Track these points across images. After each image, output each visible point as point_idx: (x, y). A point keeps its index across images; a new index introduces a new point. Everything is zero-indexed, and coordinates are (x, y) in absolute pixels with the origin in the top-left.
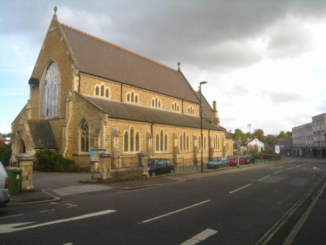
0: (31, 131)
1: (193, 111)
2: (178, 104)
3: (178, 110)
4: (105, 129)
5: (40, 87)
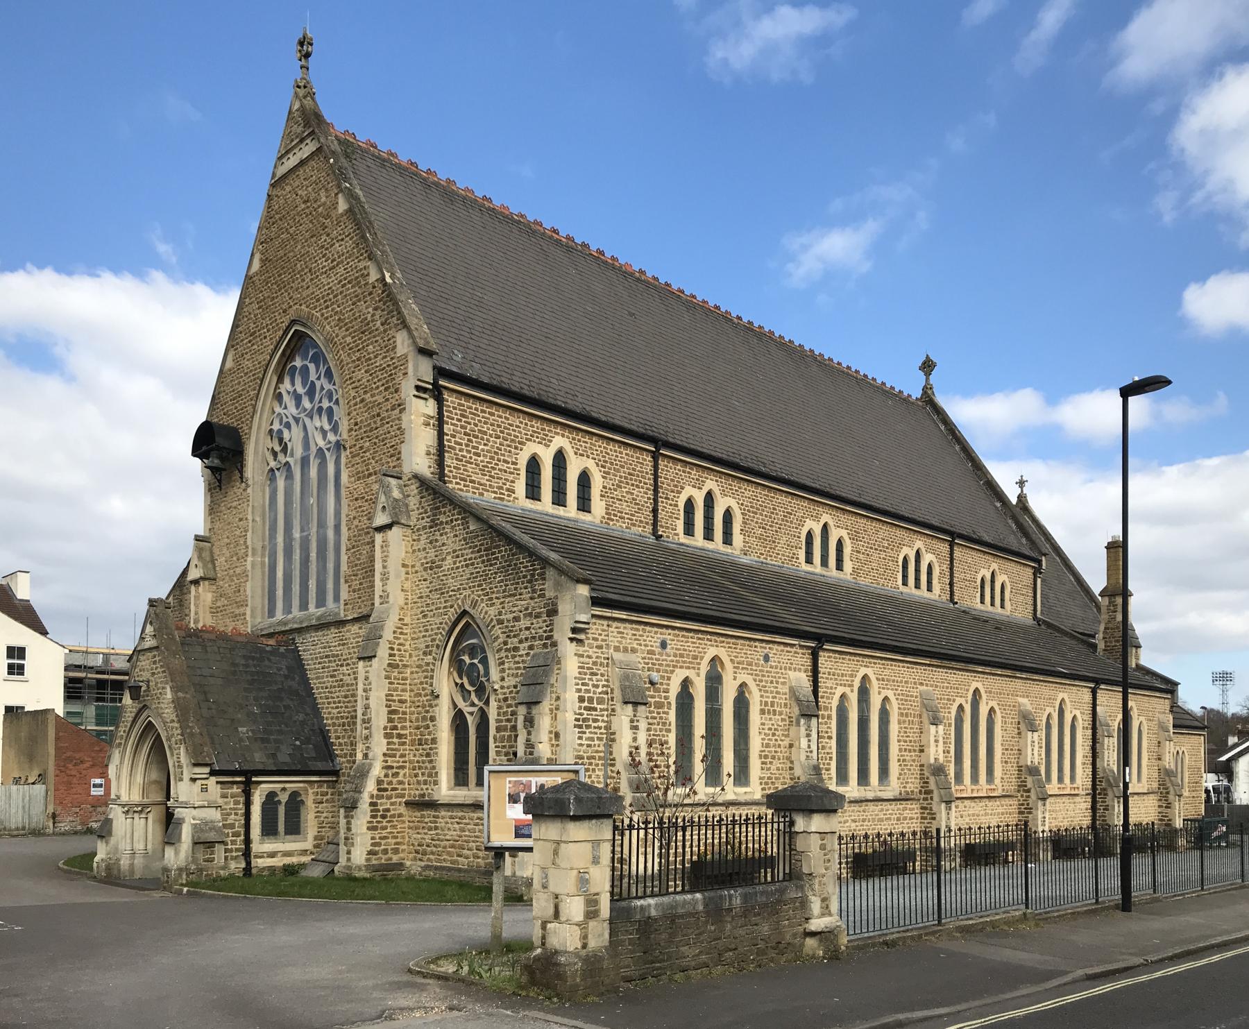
1: (1001, 591)
2: (927, 558)
3: (929, 589)
5: (249, 472)
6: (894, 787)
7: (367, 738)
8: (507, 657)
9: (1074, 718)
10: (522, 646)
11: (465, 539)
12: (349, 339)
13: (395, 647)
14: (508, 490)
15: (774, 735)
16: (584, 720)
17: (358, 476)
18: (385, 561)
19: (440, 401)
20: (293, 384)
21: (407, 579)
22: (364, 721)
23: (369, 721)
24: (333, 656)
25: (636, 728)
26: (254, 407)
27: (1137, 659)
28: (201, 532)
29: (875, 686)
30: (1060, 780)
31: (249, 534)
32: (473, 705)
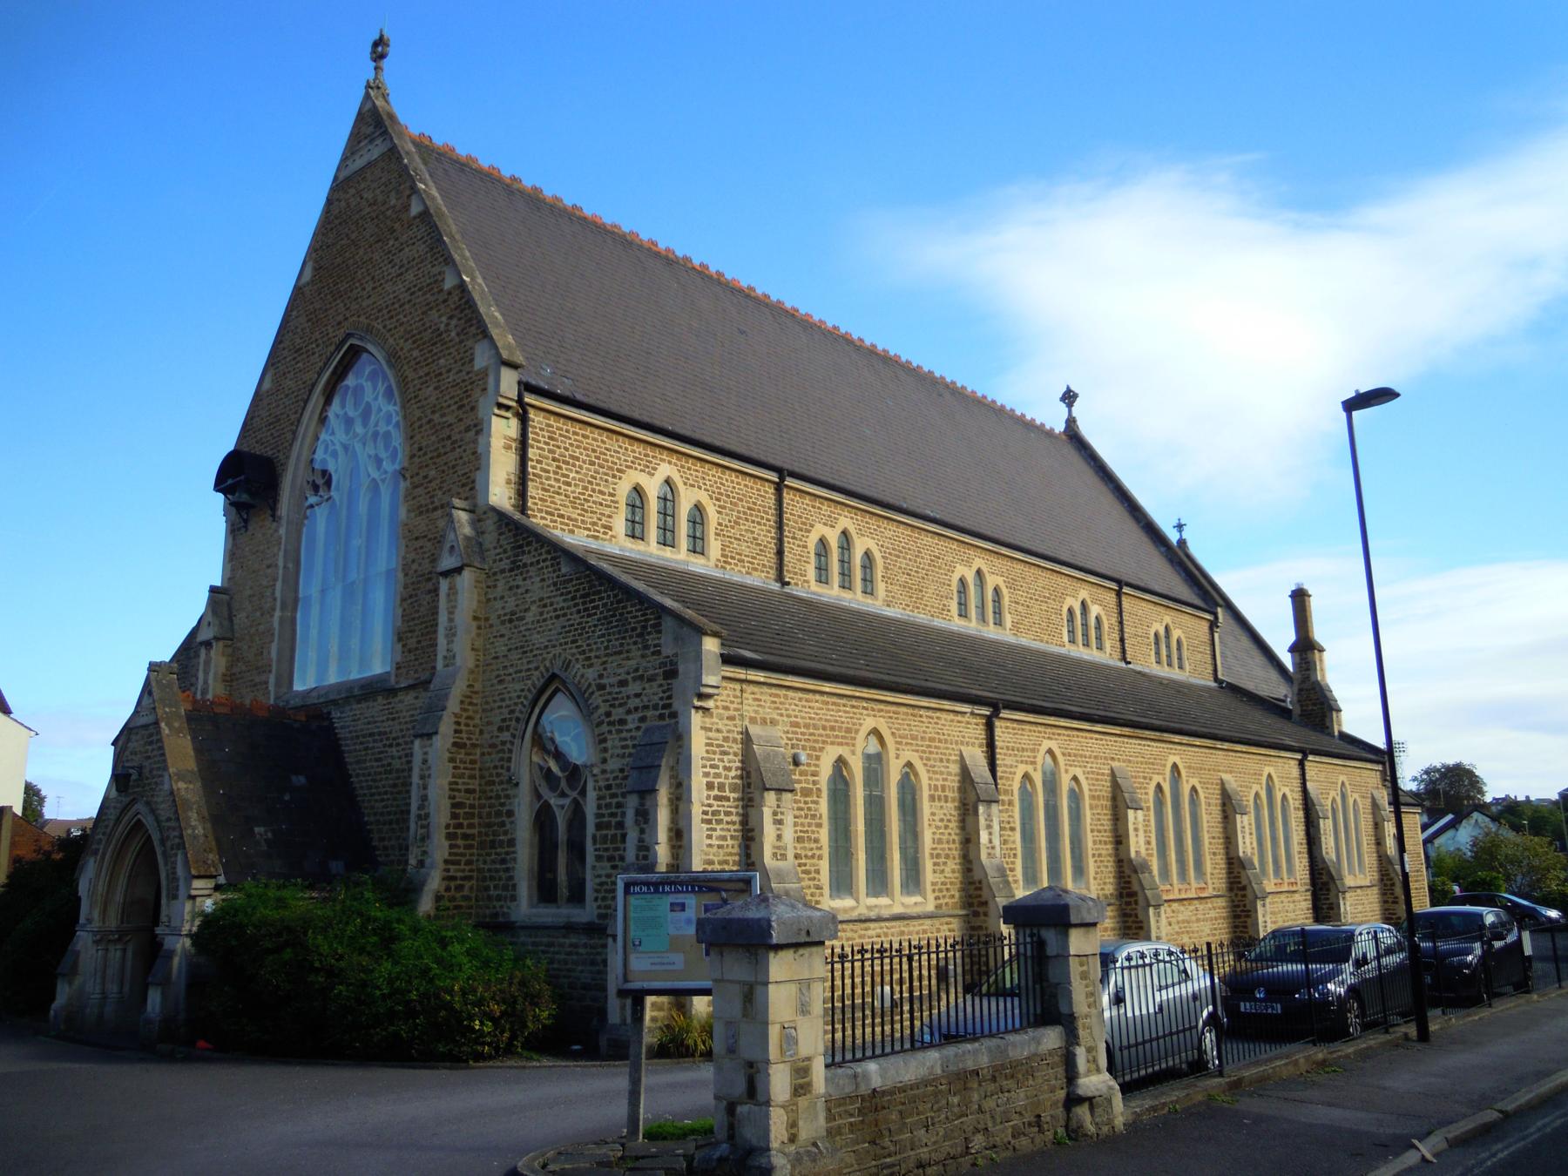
0: (210, 772)
1: (1162, 645)
2: (1095, 610)
4: (708, 742)
7: (423, 839)
8: (610, 732)
10: (629, 718)
11: (555, 584)
12: (416, 353)
13: (463, 721)
14: (604, 527)
15: (946, 827)
16: (715, 813)
18: (451, 613)
19: (524, 420)
20: (343, 406)
21: (478, 635)
22: (419, 817)
23: (427, 816)
24: (380, 734)
25: (780, 822)
26: (294, 433)
27: (1340, 725)
28: (218, 583)
31: (279, 585)
32: (563, 795)
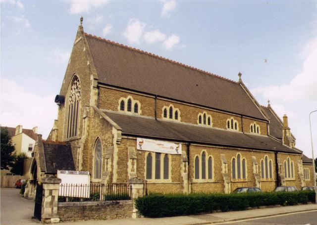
1: (257, 131)
2: (235, 121)
3: (236, 129)
5: (65, 105)
6: (213, 180)
9: (270, 161)
17: (83, 106)
28: (57, 119)
29: (207, 154)
30: (267, 177)
